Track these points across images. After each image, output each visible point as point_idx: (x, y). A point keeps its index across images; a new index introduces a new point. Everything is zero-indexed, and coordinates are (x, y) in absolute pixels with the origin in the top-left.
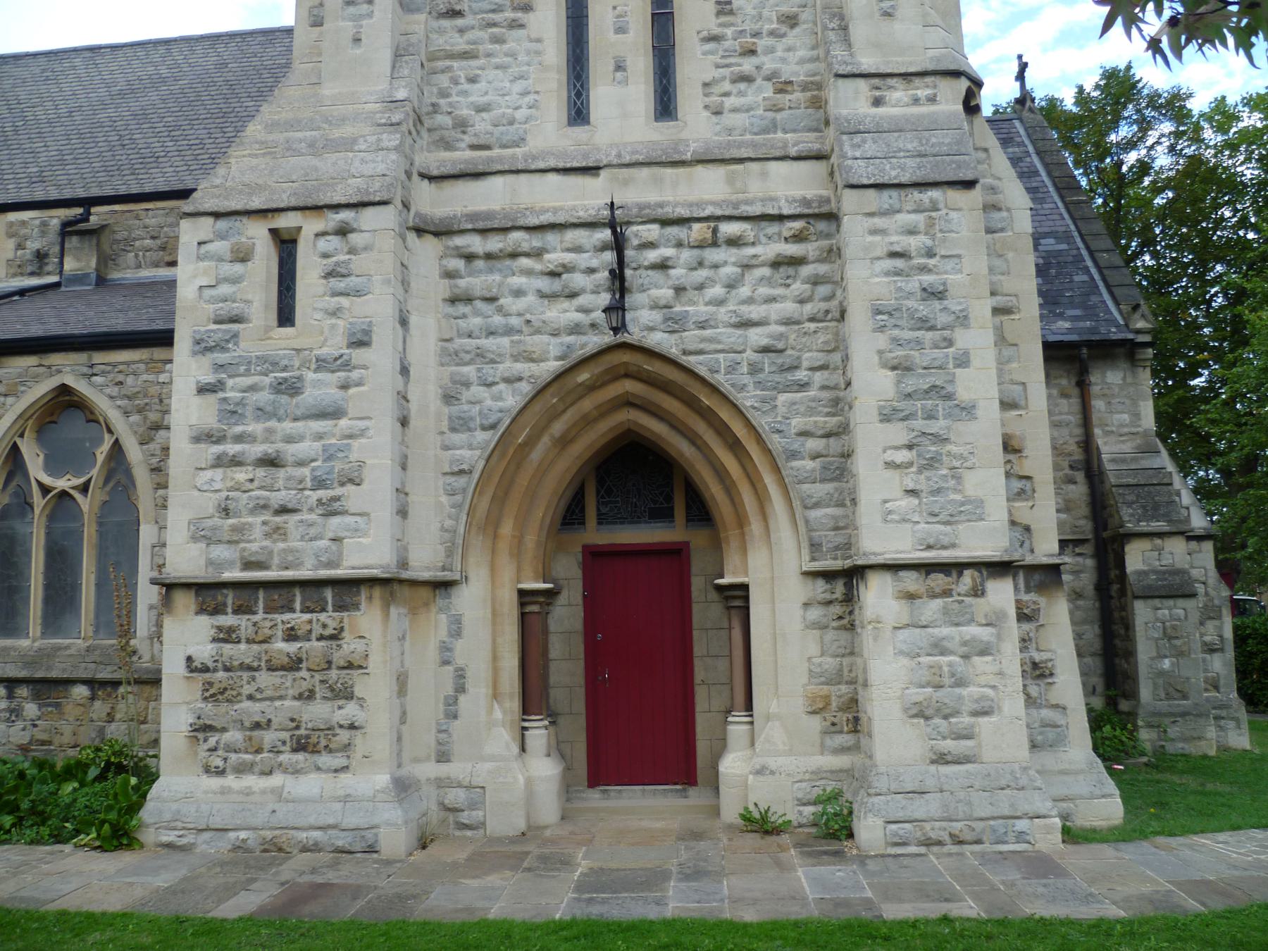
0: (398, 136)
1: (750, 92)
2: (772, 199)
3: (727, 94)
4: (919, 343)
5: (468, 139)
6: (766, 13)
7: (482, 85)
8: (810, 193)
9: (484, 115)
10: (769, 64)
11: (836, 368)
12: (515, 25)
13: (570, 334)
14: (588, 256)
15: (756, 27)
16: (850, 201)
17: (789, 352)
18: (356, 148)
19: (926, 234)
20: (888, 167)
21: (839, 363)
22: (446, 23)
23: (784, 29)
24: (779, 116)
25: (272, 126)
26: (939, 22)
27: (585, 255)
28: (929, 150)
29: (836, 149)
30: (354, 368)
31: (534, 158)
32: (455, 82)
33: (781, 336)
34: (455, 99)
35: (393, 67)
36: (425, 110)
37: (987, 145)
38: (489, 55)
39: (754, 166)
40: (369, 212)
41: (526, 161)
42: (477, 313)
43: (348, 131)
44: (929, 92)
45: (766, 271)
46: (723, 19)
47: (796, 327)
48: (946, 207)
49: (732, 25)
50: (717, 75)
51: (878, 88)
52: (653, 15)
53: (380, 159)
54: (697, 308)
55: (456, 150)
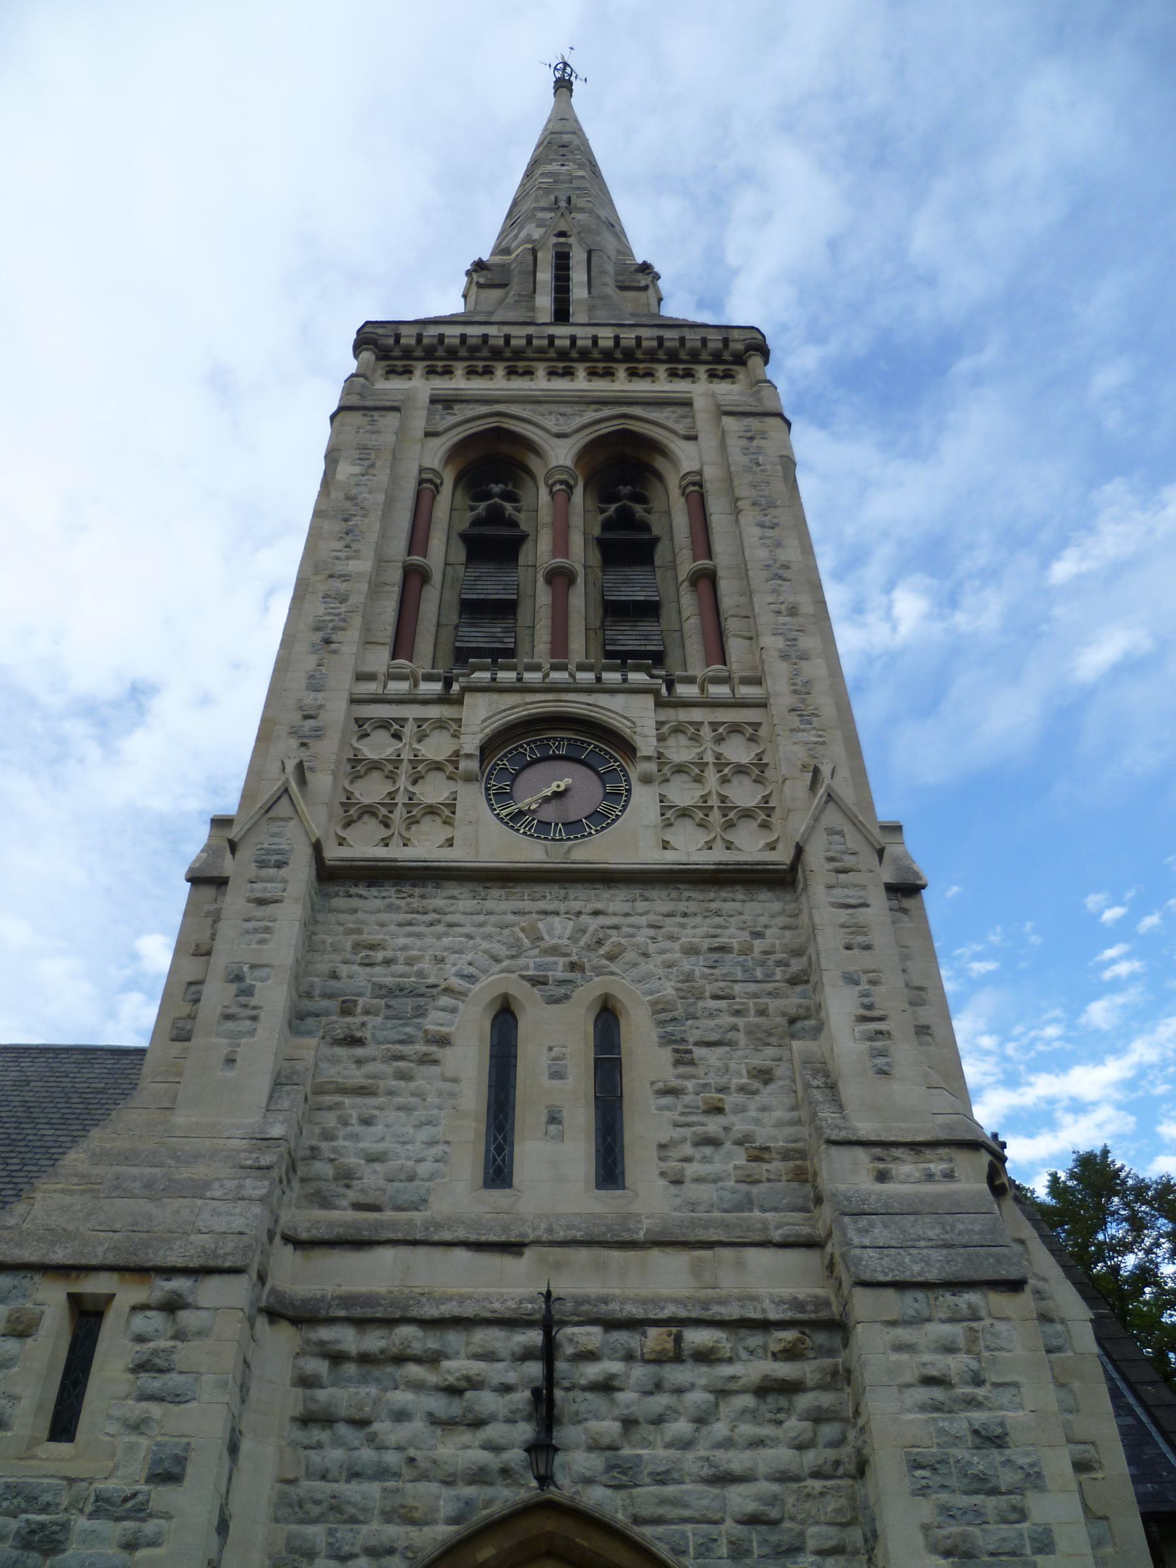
0: (266, 1183)
1: (717, 1158)
2: (753, 1298)
3: (688, 1160)
4: (977, 1512)
5: (352, 1195)
6: (733, 1065)
7: (378, 1129)
8: (803, 1292)
9: (377, 1166)
10: (740, 1126)
11: (855, 1552)
12: (427, 1060)
13: (470, 1483)
14: (501, 1370)
15: (723, 1081)
16: (863, 1303)
17: (787, 1524)
18: (208, 1194)
19: (968, 1352)
20: (907, 1260)
21: (860, 1544)
22: (341, 1051)
23: (756, 1085)
24: (755, 1190)
25: (98, 1158)
26: (943, 1085)
27: (500, 1366)
28: (958, 1240)
29: (836, 1234)
30: (151, 1516)
31: (438, 1226)
32: (345, 1122)
33: (774, 1500)
34: (341, 1143)
35: (271, 1097)
36: (301, 1153)
37: (1023, 1236)
38: (391, 1093)
39: (727, 1253)
40: (214, 1282)
41: (427, 1229)
42: (338, 1442)
43: (200, 1171)
44: (944, 1166)
45: (748, 1400)
46: (682, 1070)
47: (795, 1486)
48: (990, 1315)
49: (693, 1077)
50: (675, 1136)
51: (880, 1159)
52: (596, 1060)
53: (238, 1211)
54: (653, 1453)
55: (336, 1208)
